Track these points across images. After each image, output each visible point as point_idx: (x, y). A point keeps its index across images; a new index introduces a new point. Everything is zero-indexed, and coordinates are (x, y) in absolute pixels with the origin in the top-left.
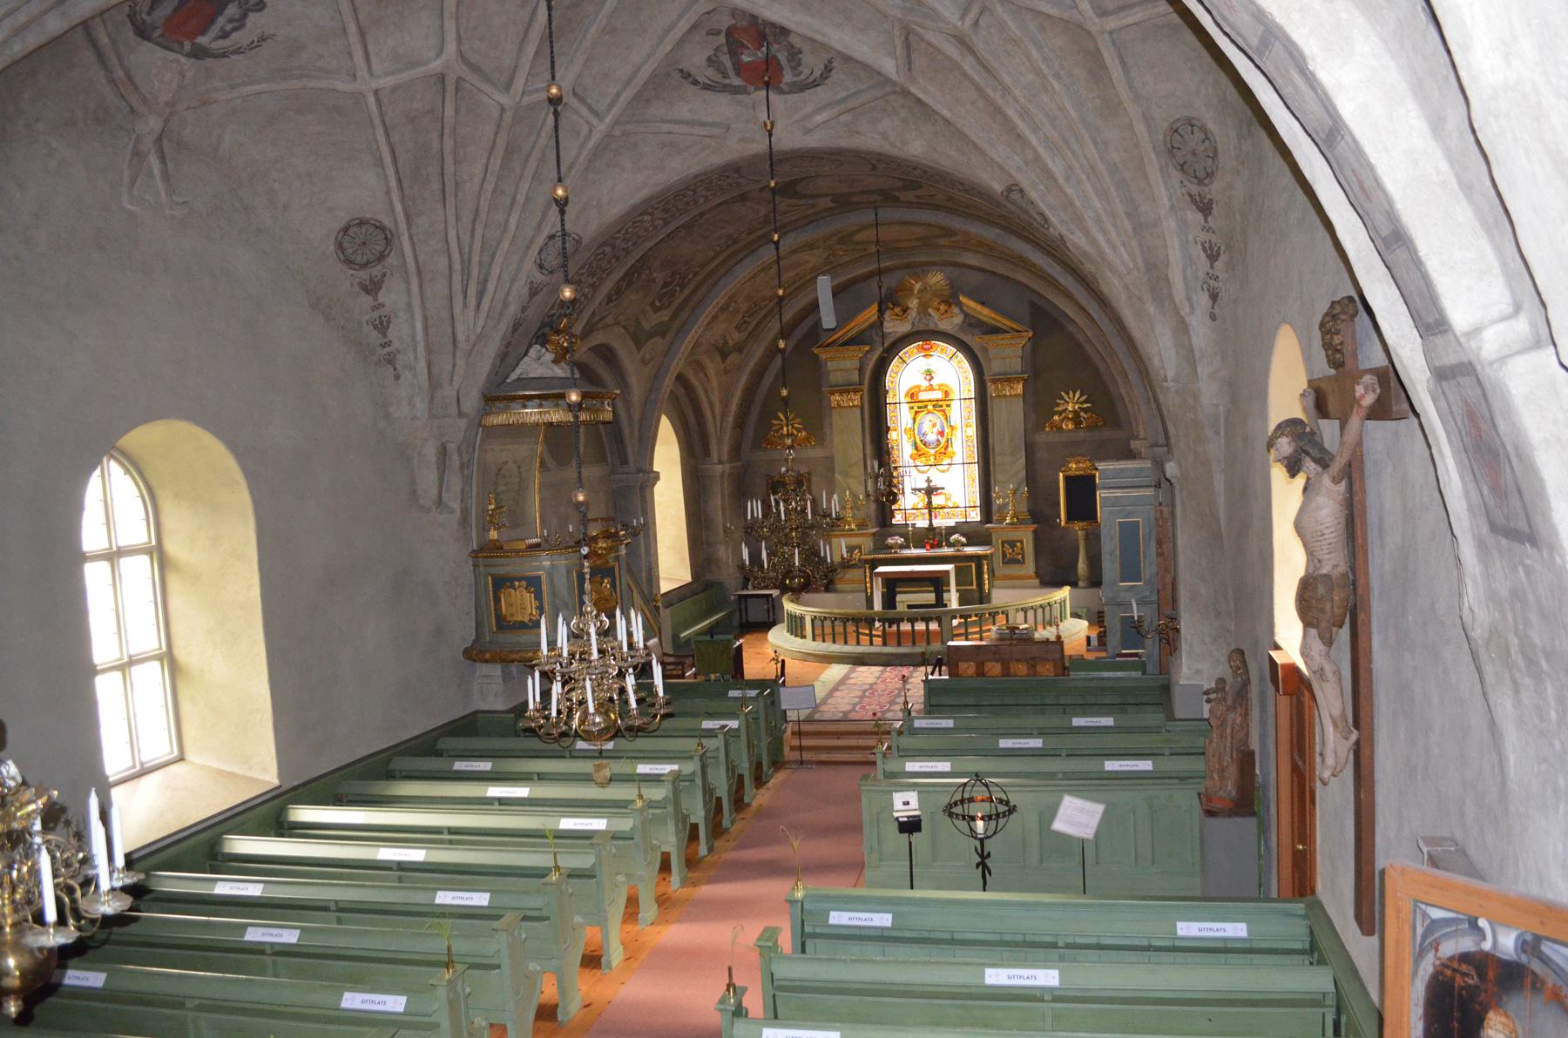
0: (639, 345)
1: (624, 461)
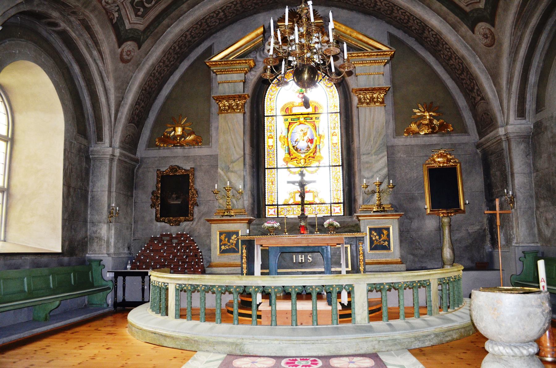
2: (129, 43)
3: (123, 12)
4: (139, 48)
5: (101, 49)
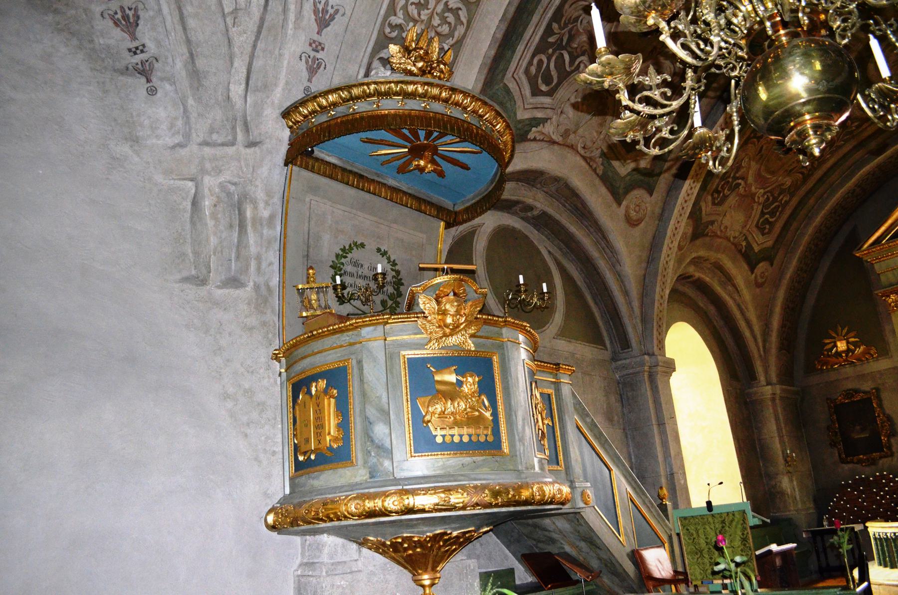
0: (618, 196)
1: (625, 343)
2: (761, 265)
3: (750, 238)
4: (772, 265)
5: (735, 282)
